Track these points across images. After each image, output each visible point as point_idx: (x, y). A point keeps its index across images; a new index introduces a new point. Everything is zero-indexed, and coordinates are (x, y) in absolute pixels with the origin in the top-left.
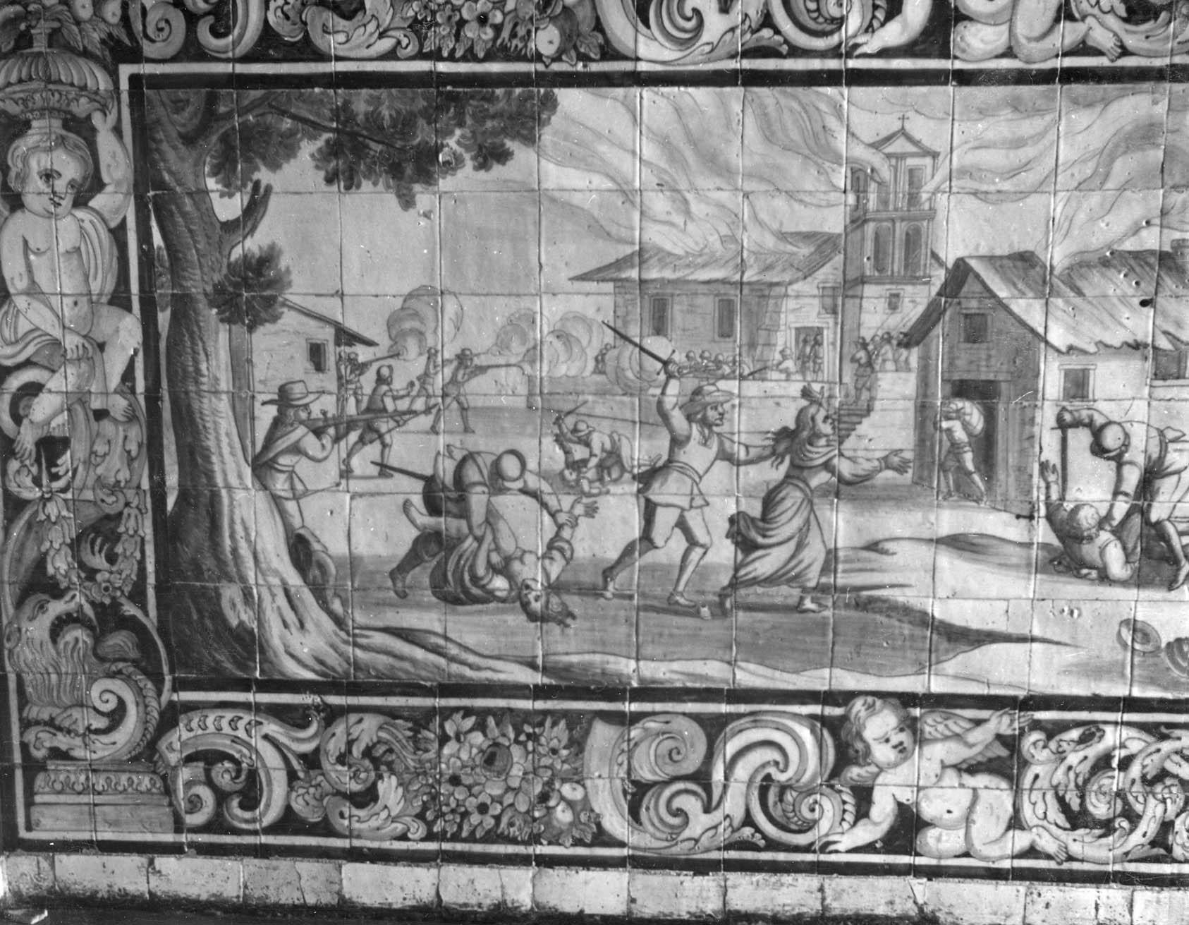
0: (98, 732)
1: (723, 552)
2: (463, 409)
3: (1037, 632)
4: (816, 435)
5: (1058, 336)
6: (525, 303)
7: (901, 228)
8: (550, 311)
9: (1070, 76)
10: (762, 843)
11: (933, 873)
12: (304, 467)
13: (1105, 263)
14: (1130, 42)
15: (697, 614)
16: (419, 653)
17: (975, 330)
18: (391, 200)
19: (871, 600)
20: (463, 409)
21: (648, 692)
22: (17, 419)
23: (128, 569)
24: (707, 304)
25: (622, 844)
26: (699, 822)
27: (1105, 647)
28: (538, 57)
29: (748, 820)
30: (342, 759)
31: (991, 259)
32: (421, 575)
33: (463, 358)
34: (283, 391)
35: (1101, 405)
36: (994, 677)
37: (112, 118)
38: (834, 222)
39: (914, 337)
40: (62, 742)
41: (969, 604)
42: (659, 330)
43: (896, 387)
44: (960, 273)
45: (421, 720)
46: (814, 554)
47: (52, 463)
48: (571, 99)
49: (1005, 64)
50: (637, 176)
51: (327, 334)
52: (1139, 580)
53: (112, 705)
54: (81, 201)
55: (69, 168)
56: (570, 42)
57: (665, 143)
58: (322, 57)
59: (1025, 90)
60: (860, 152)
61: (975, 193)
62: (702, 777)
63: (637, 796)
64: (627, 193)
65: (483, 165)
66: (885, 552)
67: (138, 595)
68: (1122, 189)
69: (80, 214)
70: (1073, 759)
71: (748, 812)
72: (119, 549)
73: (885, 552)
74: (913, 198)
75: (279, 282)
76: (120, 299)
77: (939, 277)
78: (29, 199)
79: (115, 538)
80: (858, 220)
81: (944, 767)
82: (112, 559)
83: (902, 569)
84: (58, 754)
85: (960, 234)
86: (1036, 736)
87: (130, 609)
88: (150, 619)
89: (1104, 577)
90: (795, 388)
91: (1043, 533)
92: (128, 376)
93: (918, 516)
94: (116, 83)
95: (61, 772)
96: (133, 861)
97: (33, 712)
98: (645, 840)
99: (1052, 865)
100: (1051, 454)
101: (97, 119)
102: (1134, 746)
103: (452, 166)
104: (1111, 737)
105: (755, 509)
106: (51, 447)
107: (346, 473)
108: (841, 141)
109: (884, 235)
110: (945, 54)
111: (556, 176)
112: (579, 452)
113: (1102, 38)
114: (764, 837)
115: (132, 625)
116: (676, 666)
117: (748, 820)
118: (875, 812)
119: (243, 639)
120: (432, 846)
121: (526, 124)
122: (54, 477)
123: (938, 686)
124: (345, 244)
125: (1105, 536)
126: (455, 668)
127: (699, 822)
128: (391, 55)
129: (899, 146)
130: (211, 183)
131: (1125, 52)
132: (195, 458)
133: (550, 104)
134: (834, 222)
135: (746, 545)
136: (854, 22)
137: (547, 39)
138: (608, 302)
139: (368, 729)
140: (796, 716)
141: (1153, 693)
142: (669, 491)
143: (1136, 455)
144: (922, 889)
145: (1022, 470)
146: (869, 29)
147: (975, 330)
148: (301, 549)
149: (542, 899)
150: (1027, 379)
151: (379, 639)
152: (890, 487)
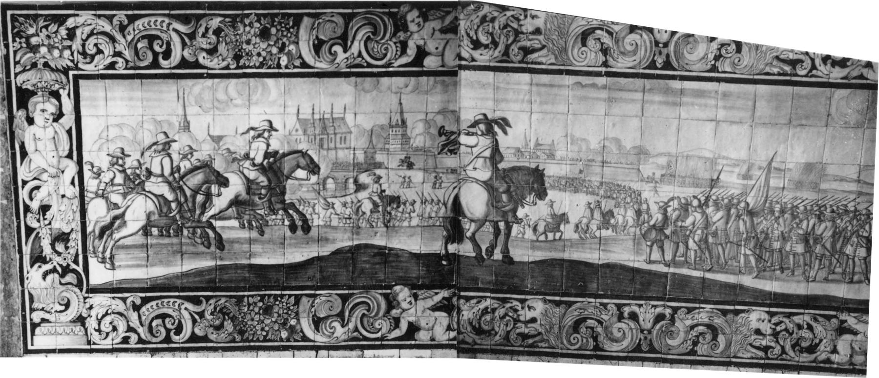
0: (61, 312)
10: (365, 64)
22: (31, 199)
23: (72, 251)
26: (341, 56)
29: (360, 55)
30: (204, 36)
37: (66, 92)
40: (47, 316)
45: (234, 18)
47: (44, 215)
53: (65, 302)
54: (56, 120)
55: (51, 107)
63: (317, 47)
67: (76, 262)
69: (55, 124)
71: (360, 52)
72: (69, 245)
76: (70, 156)
78: (36, 120)
79: (68, 240)
82: (67, 248)
84: (44, 320)
87: (73, 266)
88: (80, 269)
92: (73, 183)
94: (68, 78)
95: (44, 328)
97: (35, 305)
98: (322, 65)
99: (470, 346)
101: (61, 91)
102: (496, 306)
106: (45, 208)
114: (366, 62)
115: (74, 271)
117: (360, 55)
118: (409, 51)
120: (240, 71)
122: (45, 219)
127: (341, 56)
139: (215, 23)
146: (390, 331)
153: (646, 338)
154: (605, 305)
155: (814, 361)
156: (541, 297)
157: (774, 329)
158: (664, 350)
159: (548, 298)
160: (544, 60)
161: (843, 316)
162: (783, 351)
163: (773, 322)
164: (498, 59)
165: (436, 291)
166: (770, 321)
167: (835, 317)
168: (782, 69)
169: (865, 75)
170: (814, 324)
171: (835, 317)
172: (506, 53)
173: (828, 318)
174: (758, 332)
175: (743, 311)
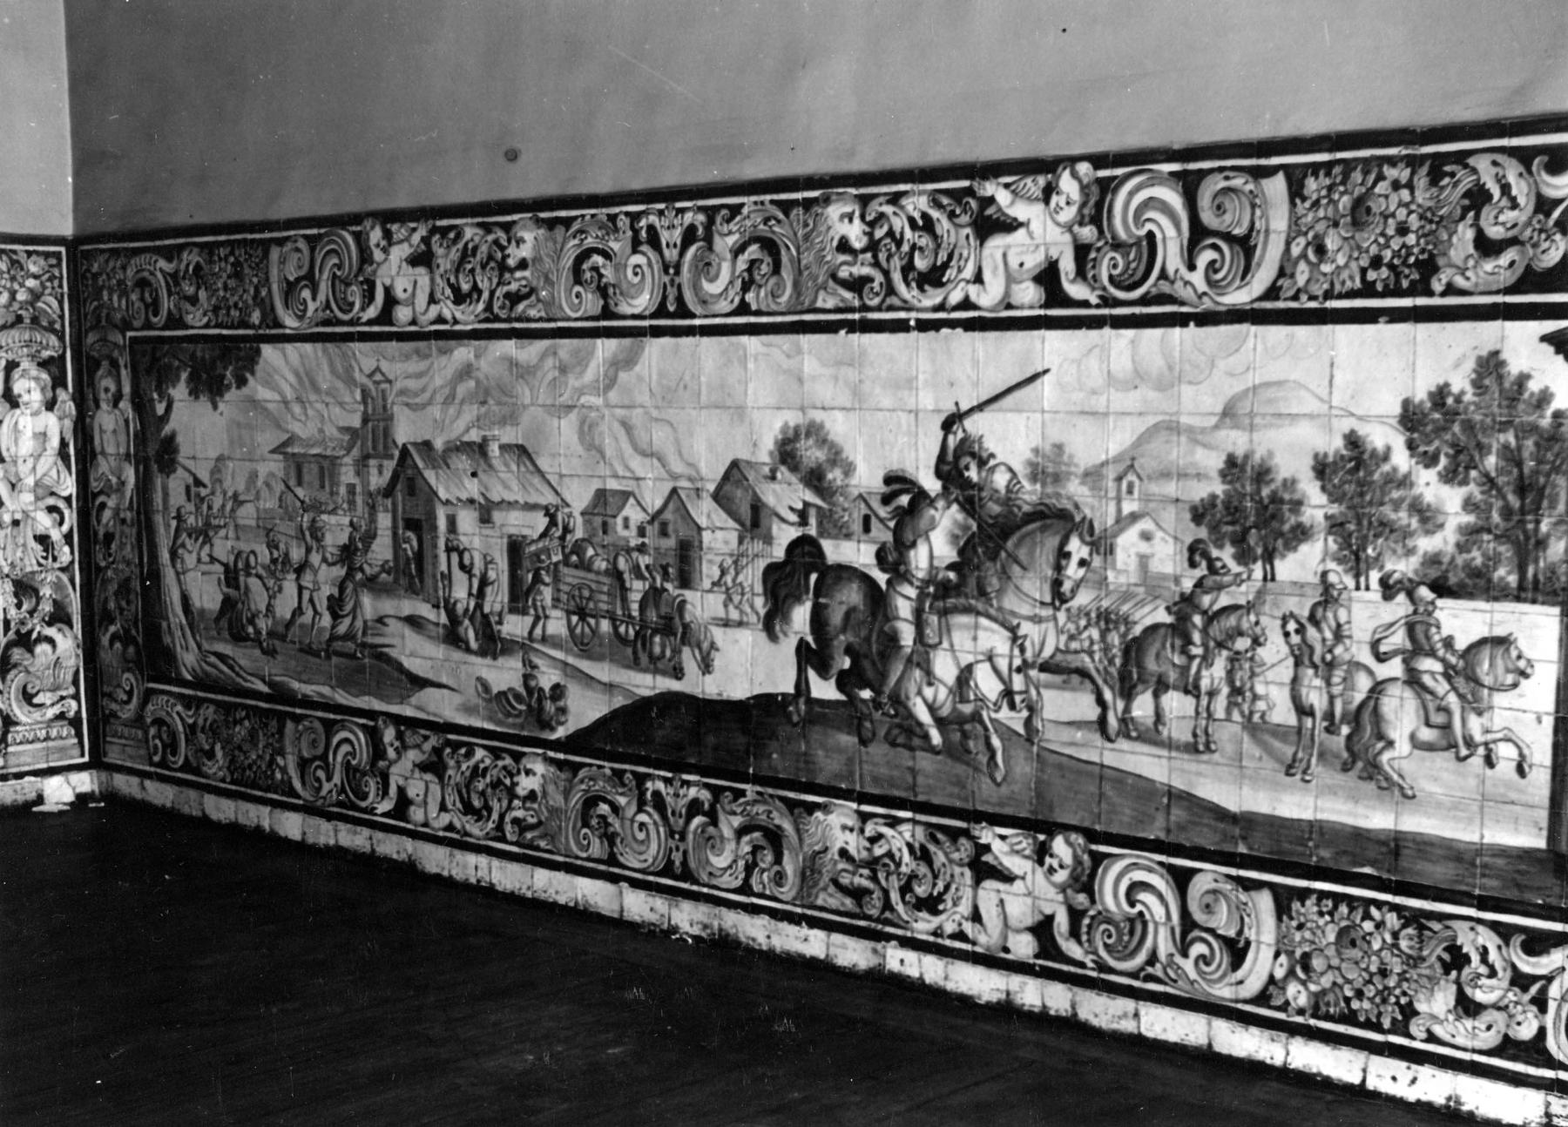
1: (326, 620)
2: (236, 526)
3: (444, 680)
4: (357, 549)
5: (443, 494)
6: (254, 465)
7: (382, 424)
8: (263, 469)
9: (439, 335)
11: (414, 835)
12: (186, 556)
13: (457, 449)
14: (458, 315)
15: (319, 656)
16: (225, 669)
17: (411, 490)
18: (209, 405)
19: (382, 654)
20: (236, 526)
21: (307, 702)
24: (315, 468)
25: (299, 797)
27: (471, 694)
28: (253, 327)
31: (415, 444)
32: (224, 623)
33: (235, 496)
34: (178, 510)
35: (462, 538)
36: (432, 708)
38: (356, 422)
39: (388, 492)
41: (418, 661)
42: (300, 484)
43: (384, 521)
44: (405, 452)
46: (359, 624)
48: (267, 350)
49: (413, 328)
50: (290, 394)
51: (191, 480)
52: (482, 653)
56: (263, 320)
57: (297, 374)
58: (187, 327)
59: (422, 345)
60: (365, 380)
61: (407, 405)
62: (324, 757)
64: (285, 402)
65: (238, 387)
66: (385, 624)
68: (462, 402)
70: (464, 767)
73: (385, 624)
74: (385, 407)
75: (175, 451)
77: (397, 453)
80: (365, 421)
81: (415, 765)
83: (393, 635)
85: (405, 431)
86: (448, 750)
89: (468, 650)
90: (346, 520)
91: (444, 619)
93: (395, 602)
96: (135, 780)
100: (443, 567)
103: (228, 387)
104: (480, 753)
105: (336, 592)
107: (199, 560)
108: (357, 375)
109: (373, 431)
110: (391, 324)
111: (264, 393)
112: (276, 554)
113: (447, 314)
116: (314, 687)
119: (1042, 512)
121: (251, 360)
123: (408, 711)
124: (197, 424)
125: (467, 622)
126: (239, 680)
128: (207, 326)
129: (378, 377)
130: (155, 396)
131: (456, 322)
132: (154, 556)
133: (258, 352)
134: (356, 422)
135: (336, 617)
136: (357, 306)
137: (256, 317)
138: (282, 465)
140: (357, 724)
141: (491, 727)
142: (307, 579)
143: (476, 571)
144: (409, 845)
145: (434, 576)
146: (363, 309)
147: (411, 490)
148: (185, 599)
149: (277, 828)
150: (432, 517)
151: (213, 659)
152: (385, 584)
153: (672, 281)
154: (613, 218)
155: (941, 307)
156: (540, 751)
157: (870, 235)
158: (704, 877)
159: (551, 754)
160: (533, 313)
161: (986, 835)
162: (888, 905)
163: (867, 834)
164: (482, 317)
165: (413, 225)
166: (862, 831)
167: (970, 192)
168: (843, 300)
169: (973, 298)
170: (932, 848)
171: (966, 833)
172: (500, 827)
173: (954, 835)
174: (844, 246)
175: (817, 806)
